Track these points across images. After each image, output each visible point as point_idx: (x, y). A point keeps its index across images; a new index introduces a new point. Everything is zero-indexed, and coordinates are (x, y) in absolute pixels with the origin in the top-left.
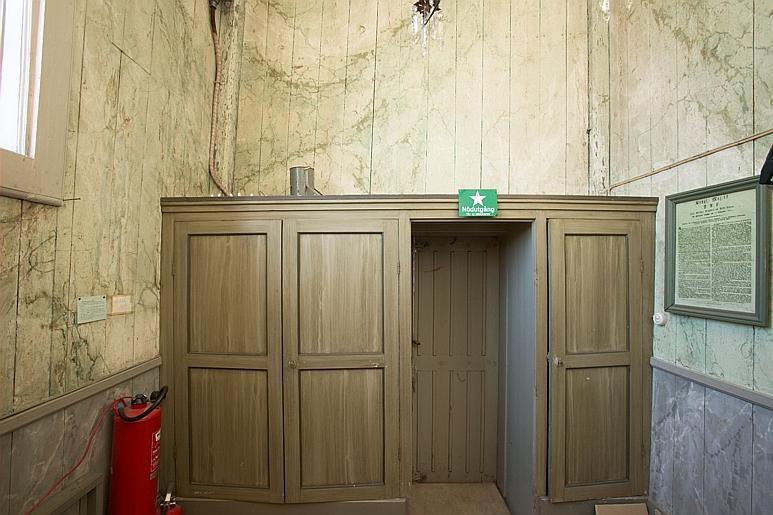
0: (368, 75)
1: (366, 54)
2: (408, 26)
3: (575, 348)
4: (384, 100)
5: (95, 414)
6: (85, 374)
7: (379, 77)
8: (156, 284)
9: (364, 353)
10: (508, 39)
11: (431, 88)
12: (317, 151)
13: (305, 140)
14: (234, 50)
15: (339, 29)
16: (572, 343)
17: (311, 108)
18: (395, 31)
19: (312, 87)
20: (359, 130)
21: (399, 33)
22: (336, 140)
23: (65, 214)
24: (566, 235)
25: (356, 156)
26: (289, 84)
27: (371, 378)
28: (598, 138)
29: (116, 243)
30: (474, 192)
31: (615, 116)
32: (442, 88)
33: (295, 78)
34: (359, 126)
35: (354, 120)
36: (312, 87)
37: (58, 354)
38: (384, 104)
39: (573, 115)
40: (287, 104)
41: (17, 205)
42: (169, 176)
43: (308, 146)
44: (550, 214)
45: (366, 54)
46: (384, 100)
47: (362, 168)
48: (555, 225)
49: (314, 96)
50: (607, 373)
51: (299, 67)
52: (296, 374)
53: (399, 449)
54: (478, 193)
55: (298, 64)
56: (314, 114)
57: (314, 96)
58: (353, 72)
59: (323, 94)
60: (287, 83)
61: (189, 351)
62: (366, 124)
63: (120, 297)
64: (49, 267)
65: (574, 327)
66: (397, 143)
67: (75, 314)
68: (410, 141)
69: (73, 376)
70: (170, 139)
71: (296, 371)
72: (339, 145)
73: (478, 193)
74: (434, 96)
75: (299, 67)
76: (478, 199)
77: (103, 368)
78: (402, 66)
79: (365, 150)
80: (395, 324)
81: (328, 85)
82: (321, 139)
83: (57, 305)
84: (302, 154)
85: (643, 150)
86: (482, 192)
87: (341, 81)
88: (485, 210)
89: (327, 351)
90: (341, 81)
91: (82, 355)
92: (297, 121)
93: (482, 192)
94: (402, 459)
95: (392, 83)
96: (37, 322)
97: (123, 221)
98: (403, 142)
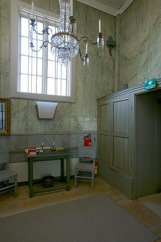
5: (82, 137)
6: (80, 130)
8: (96, 116)
9: (125, 133)
14: (117, 57)
20: (144, 66)
21: (156, 25)
22: (139, 72)
23: (76, 104)
26: (128, 60)
29: (86, 108)
37: (76, 126)
41: (70, 103)
42: (99, 94)
47: (145, 79)
52: (113, 137)
61: (113, 132)
63: (87, 118)
64: (74, 112)
67: (78, 120)
69: (78, 129)
70: (98, 86)
71: (112, 136)
77: (83, 130)
83: (75, 118)
89: (118, 132)
91: (80, 126)
96: (73, 120)
97: (87, 104)
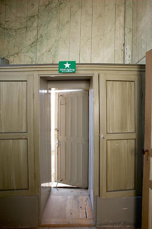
0: (35, 25)
1: (34, 16)
2: (51, 4)
3: (111, 131)
4: (41, 35)
7: (39, 25)
10: (92, 8)
11: (60, 29)
12: (15, 55)
13: (10, 51)
15: (24, 5)
16: (110, 129)
17: (12, 38)
18: (46, 6)
19: (13, 30)
20: (31, 47)
22: (23, 51)
24: (106, 81)
25: (30, 57)
26: (4, 28)
27: (22, 143)
28: (128, 47)
30: (65, 63)
31: (134, 36)
32: (65, 29)
33: (6, 26)
34: (31, 45)
35: (30, 42)
36: (13, 30)
38: (41, 36)
39: (118, 38)
40: (3, 37)
43: (11, 54)
44: (100, 72)
45: (34, 16)
46: (41, 35)
48: (102, 76)
49: (14, 33)
50: (126, 141)
51: (8, 21)
53: (35, 174)
54: (67, 63)
55: (7, 20)
56: (14, 41)
57: (14, 33)
58: (29, 24)
59: (17, 32)
60: (3, 28)
62: (34, 45)
65: (111, 121)
66: (46, 51)
68: (51, 51)
72: (24, 53)
73: (67, 63)
74: (61, 33)
75: (8, 21)
76: (67, 65)
78: (49, 21)
79: (34, 55)
80: (32, 121)
81: (19, 29)
82: (16, 51)
84: (9, 57)
85: (143, 46)
86: (69, 62)
87: (24, 27)
88: (70, 70)
90: (24, 27)
92: (7, 43)
93: (69, 62)
94: (36, 179)
95: (45, 28)
98: (48, 51)
